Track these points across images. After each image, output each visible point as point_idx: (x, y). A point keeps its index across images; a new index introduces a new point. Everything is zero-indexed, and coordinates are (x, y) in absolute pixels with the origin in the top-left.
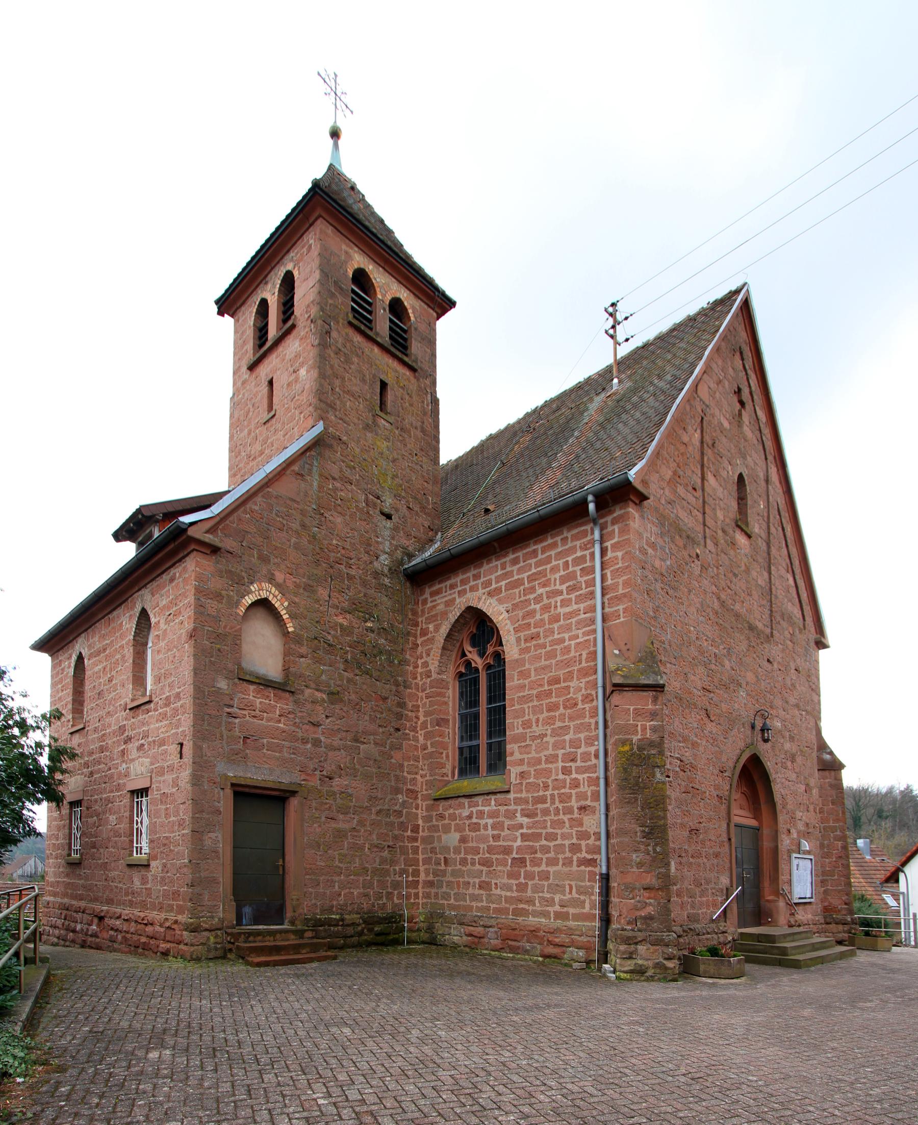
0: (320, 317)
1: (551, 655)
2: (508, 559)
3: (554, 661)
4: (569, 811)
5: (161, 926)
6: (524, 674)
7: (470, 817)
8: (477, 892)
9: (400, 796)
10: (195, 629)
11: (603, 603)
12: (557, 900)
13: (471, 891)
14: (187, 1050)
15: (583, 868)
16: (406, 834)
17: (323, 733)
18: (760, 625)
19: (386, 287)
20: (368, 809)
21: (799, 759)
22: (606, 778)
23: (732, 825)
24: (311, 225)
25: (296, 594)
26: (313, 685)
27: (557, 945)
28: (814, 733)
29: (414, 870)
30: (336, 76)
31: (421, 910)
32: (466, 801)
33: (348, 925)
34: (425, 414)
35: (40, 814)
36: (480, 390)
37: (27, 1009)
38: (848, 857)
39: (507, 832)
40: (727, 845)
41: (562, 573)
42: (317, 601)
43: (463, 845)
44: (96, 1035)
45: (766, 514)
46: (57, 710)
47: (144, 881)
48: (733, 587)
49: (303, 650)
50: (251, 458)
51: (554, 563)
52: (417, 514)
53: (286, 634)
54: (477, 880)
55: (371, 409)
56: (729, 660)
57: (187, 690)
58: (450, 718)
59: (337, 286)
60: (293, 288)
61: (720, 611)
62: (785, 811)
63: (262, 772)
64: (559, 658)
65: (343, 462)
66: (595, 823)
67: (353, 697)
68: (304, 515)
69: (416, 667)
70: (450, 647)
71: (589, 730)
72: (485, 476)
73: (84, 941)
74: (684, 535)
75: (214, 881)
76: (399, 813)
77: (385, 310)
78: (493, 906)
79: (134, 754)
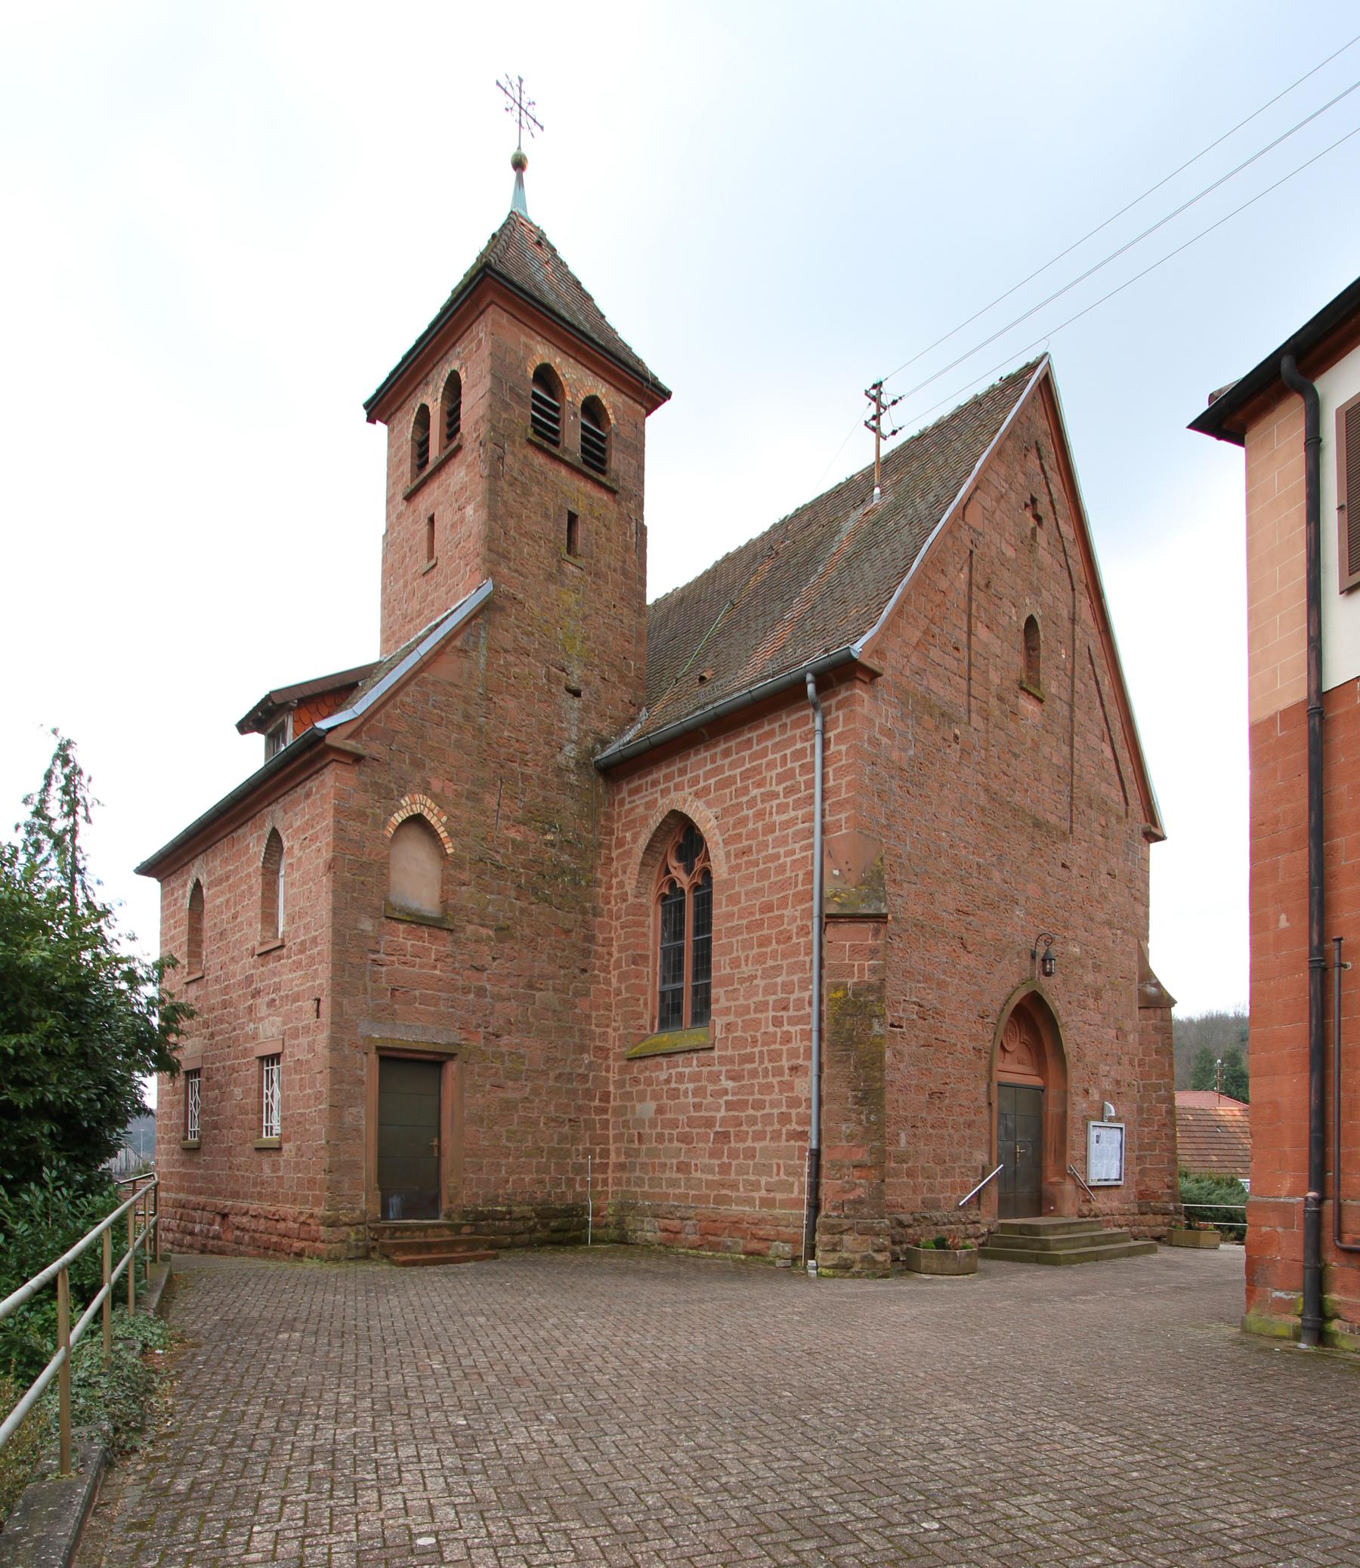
0: (491, 439)
1: (764, 875)
2: (718, 750)
3: (766, 883)
4: (778, 1072)
5: (294, 1221)
6: (733, 900)
7: (668, 1081)
8: (675, 1175)
9: (586, 1056)
10: (334, 859)
11: (823, 811)
12: (763, 1183)
13: (667, 1174)
14: (316, 1333)
15: (792, 1142)
16: (592, 1104)
17: (489, 980)
18: (1053, 819)
19: (579, 382)
20: (544, 1073)
21: (1108, 995)
22: (820, 1031)
23: (995, 1084)
24: (482, 313)
25: (456, 805)
26: (476, 920)
27: (761, 1239)
28: (1135, 958)
29: (602, 1150)
30: (521, 80)
31: (610, 1200)
32: (664, 1061)
33: (516, 1220)
34: (627, 549)
35: (151, 1089)
36: (704, 500)
37: (156, 1300)
38: (1174, 1125)
39: (710, 1099)
40: (986, 1112)
41: (779, 770)
42: (483, 812)
43: (660, 1117)
44: (226, 1322)
45: (1069, 666)
46: (172, 957)
47: (275, 1168)
48: (1011, 771)
49: (466, 876)
50: (408, 619)
51: (771, 757)
52: (614, 686)
53: (444, 856)
54: (675, 1161)
55: (556, 552)
56: (1000, 871)
57: (325, 934)
58: (650, 953)
59: (518, 381)
60: (460, 395)
61: (988, 806)
62: (1080, 1065)
63: (412, 1033)
64: (773, 879)
65: (518, 627)
66: (806, 1087)
67: (527, 931)
68: (467, 703)
69: (610, 888)
70: (651, 862)
71: (804, 971)
72: (711, 621)
73: (204, 1245)
74: (937, 711)
75: (355, 1166)
76: (584, 1078)
77: (575, 415)
78: (692, 1193)
79: (263, 1011)
